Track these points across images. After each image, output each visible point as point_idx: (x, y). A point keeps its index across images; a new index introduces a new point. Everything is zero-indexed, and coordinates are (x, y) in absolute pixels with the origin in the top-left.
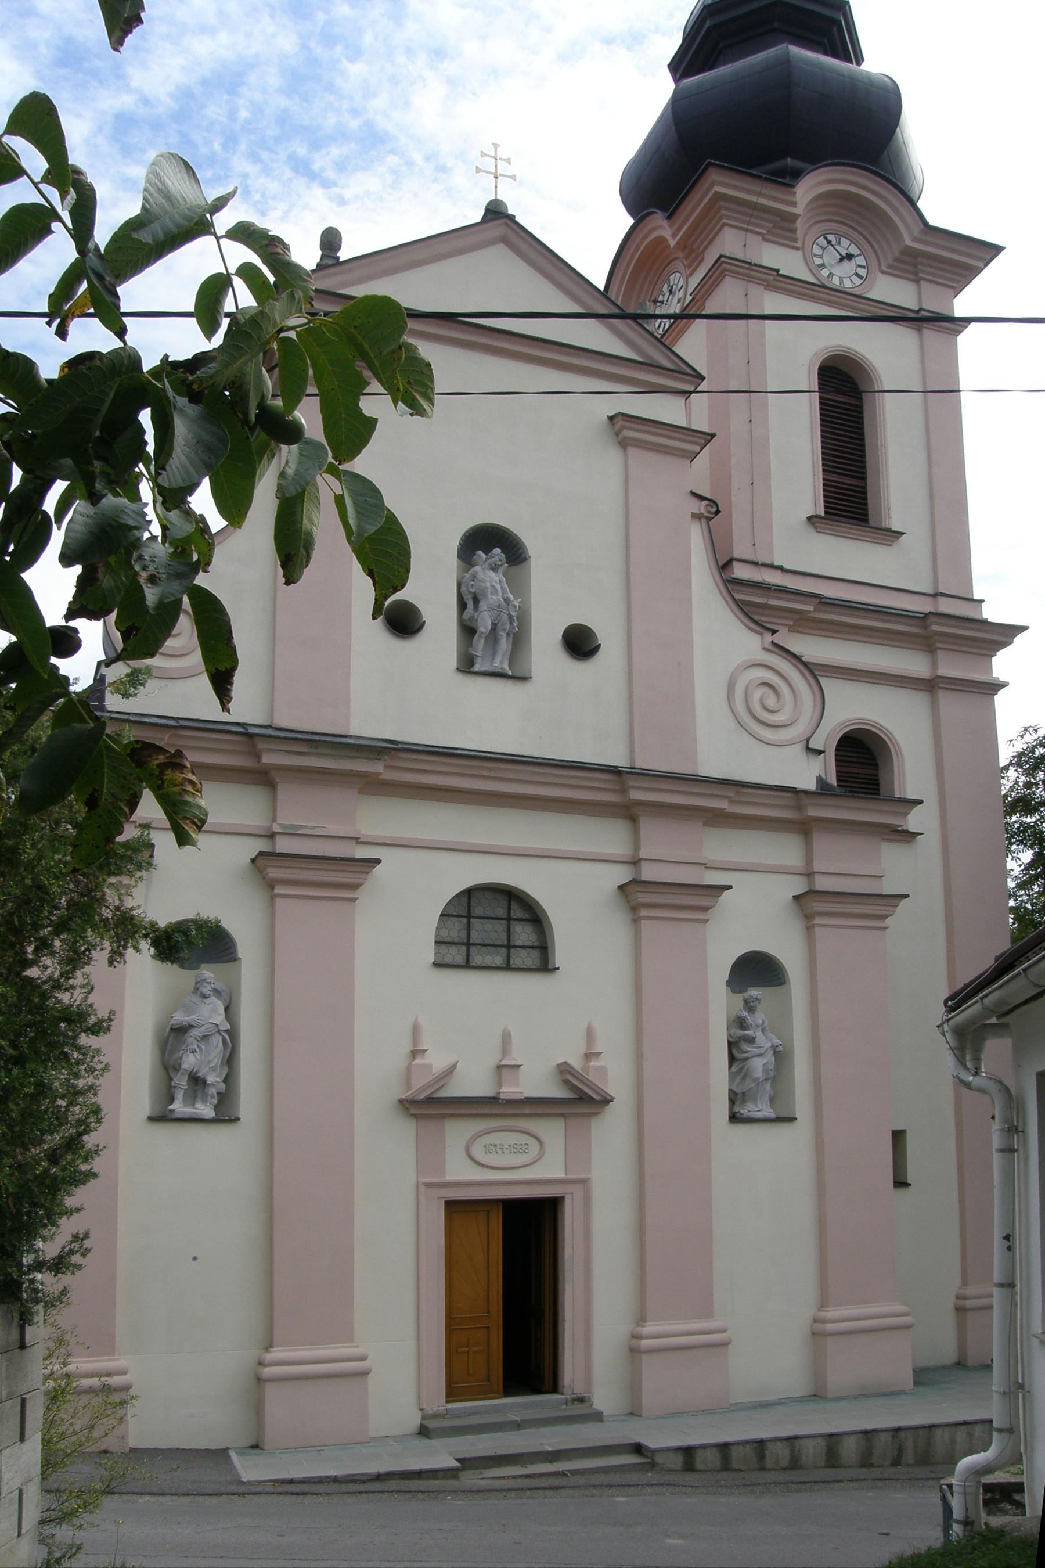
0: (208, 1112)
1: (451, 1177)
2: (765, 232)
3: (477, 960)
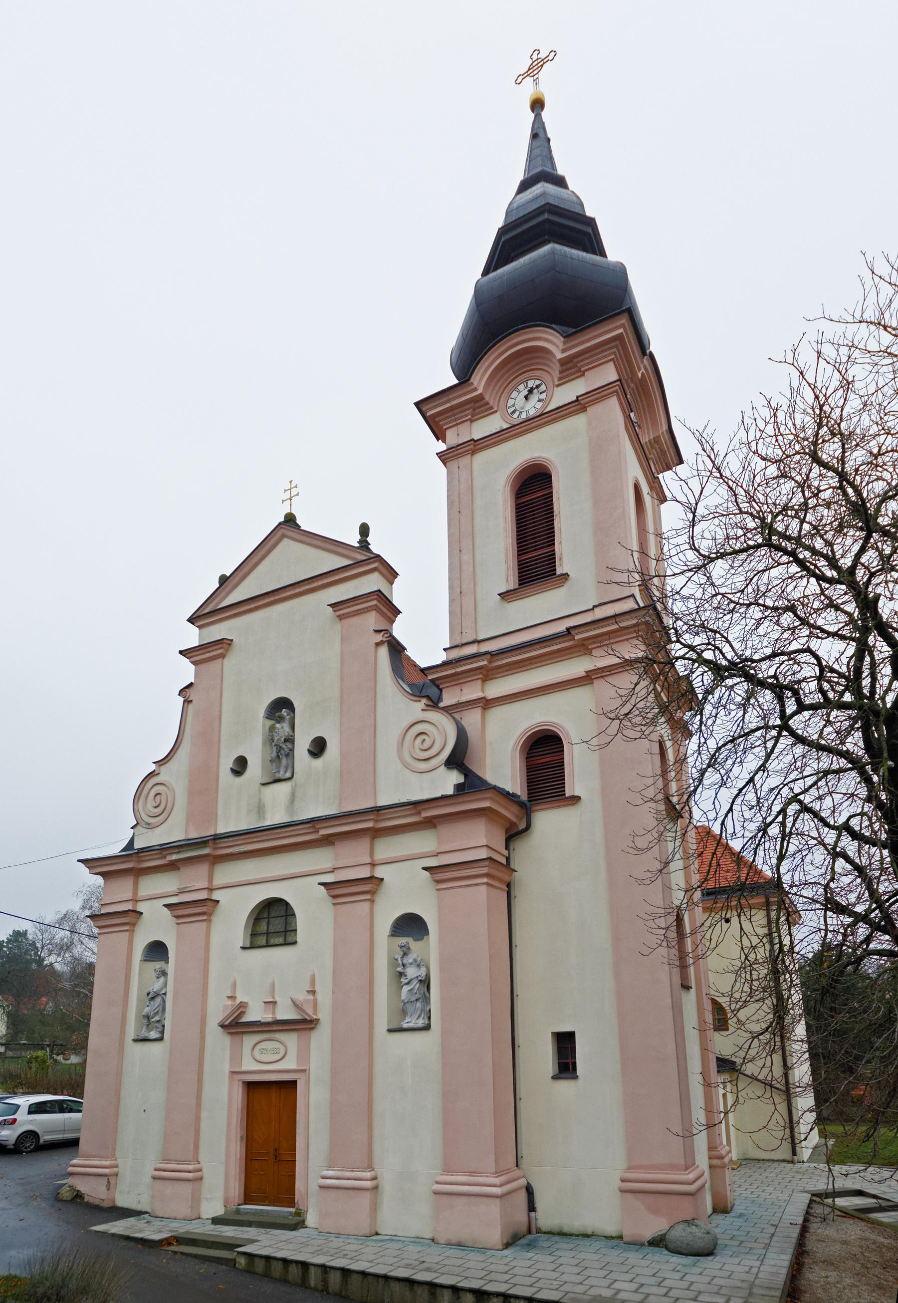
0: (153, 1034)
1: (244, 1068)
2: (470, 417)
3: (272, 941)
